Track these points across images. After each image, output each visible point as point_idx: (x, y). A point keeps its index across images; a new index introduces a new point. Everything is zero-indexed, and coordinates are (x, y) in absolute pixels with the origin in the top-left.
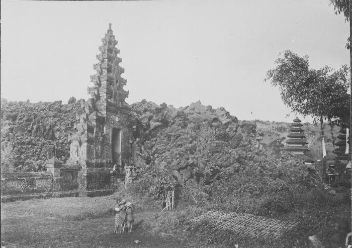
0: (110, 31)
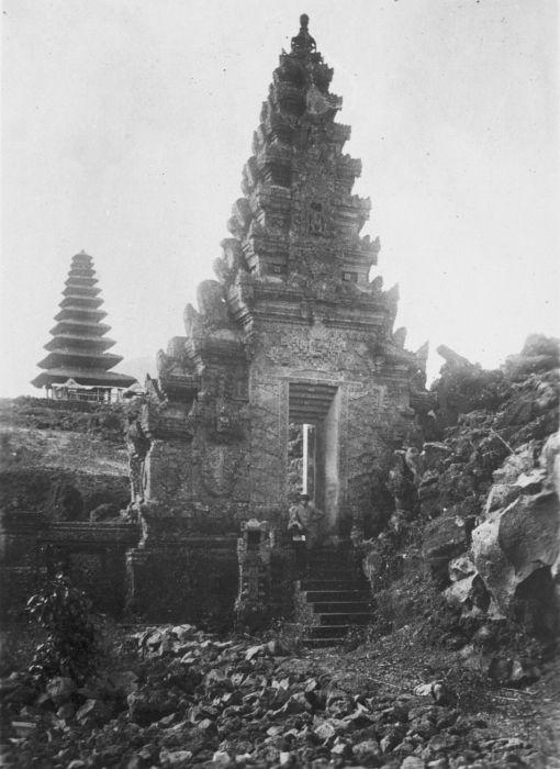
0: (303, 41)
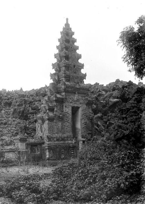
0: (67, 25)
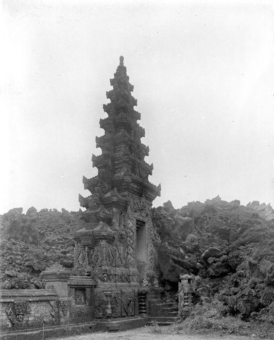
0: (121, 71)
